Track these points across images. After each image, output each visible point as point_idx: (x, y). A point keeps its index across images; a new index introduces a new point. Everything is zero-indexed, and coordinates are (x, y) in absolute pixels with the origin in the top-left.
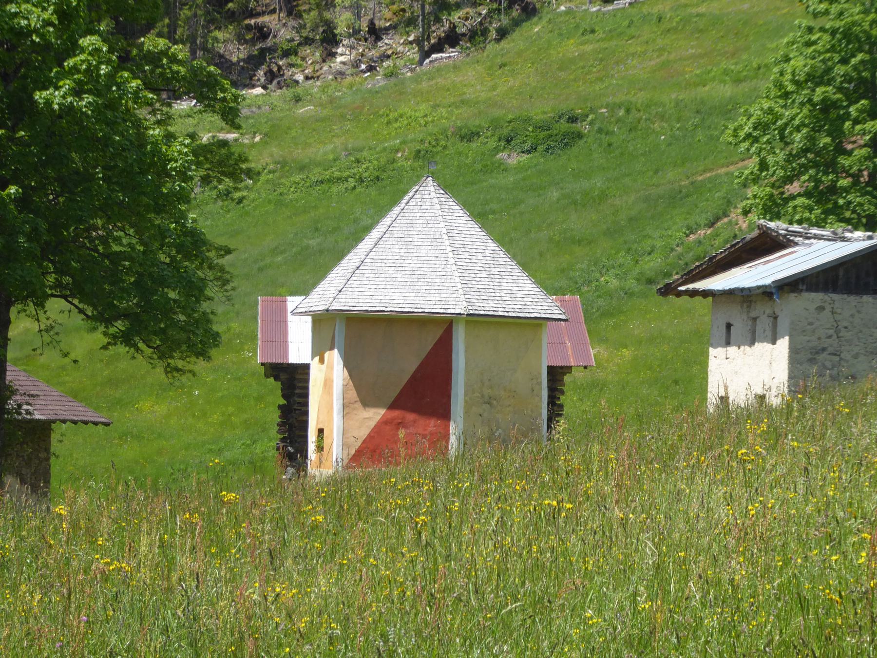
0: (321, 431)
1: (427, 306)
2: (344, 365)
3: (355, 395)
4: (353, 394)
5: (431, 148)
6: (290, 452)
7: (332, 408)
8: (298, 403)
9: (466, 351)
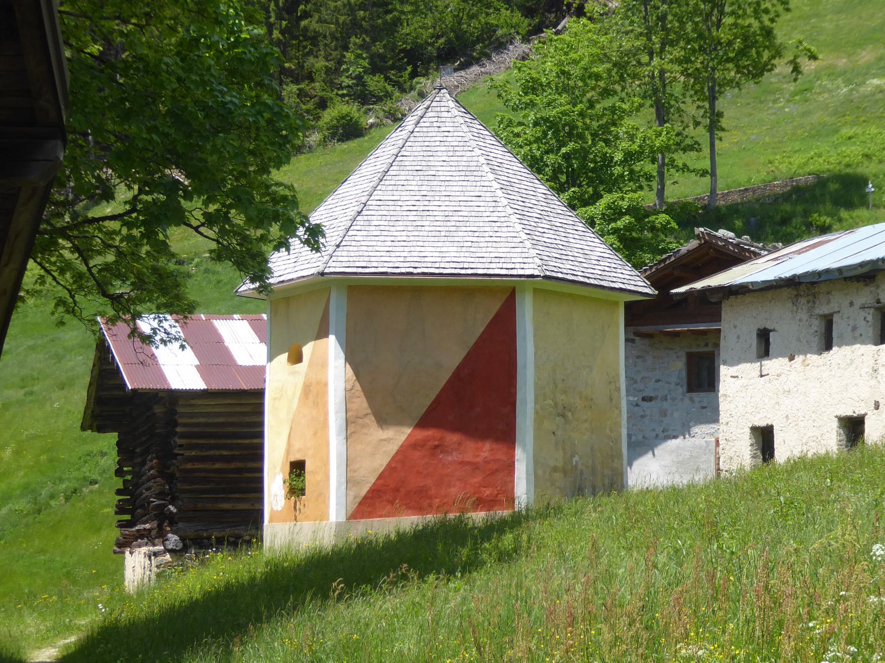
0: (297, 468)
1: (479, 266)
2: (346, 360)
3: (365, 404)
4: (361, 404)
5: (51, 288)
6: (171, 512)
7: (325, 425)
8: (181, 446)
9: (535, 336)
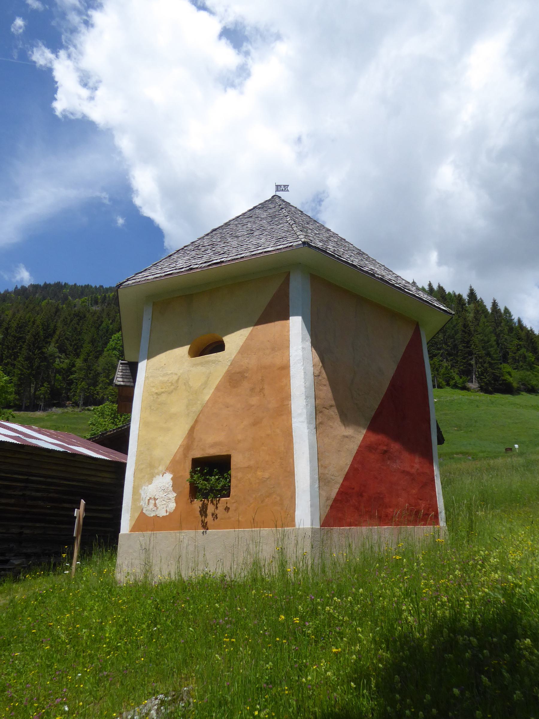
3: (330, 395)
